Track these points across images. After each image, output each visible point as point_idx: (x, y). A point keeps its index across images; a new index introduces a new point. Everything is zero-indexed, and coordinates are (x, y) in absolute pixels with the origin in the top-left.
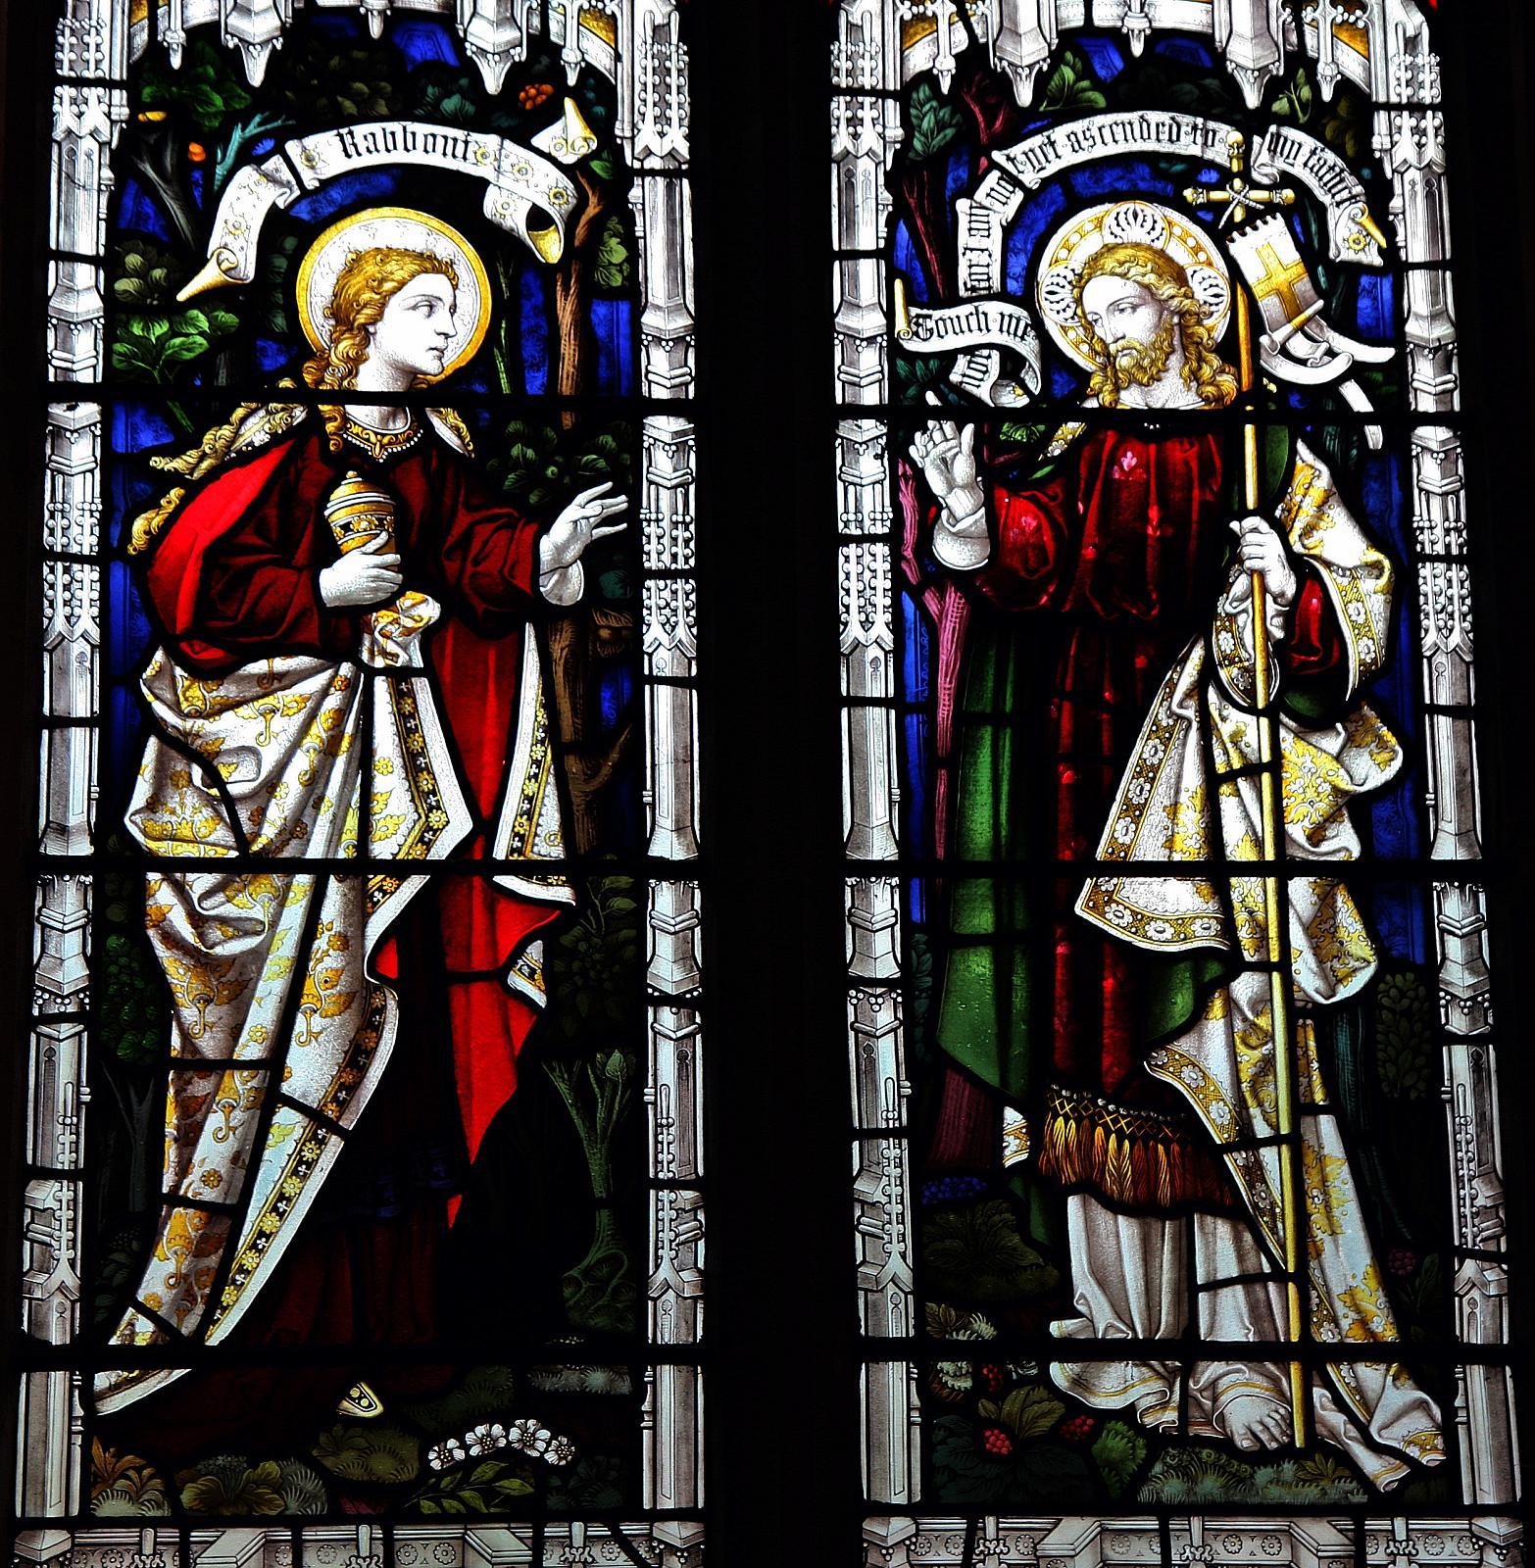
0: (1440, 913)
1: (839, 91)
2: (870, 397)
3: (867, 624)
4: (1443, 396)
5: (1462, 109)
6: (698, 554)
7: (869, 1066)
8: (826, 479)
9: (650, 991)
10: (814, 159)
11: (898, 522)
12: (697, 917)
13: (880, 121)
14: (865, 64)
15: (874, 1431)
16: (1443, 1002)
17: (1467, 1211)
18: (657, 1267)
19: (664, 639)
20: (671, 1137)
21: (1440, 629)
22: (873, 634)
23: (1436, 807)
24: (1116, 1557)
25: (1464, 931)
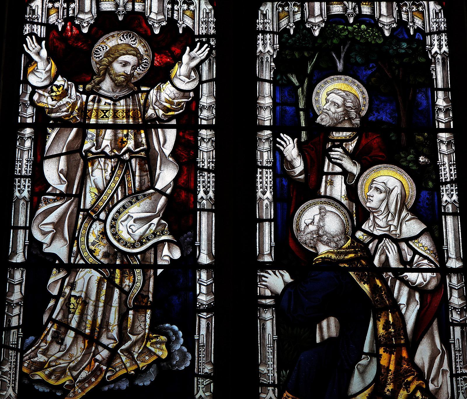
0: (440, 148)
1: (259, 32)
2: (267, 123)
3: (264, 45)
4: (447, 124)
5: (453, 33)
6: (217, 117)
7: (264, 329)
8: (254, 148)
9: (201, 66)
10: (252, 56)
11: (274, 163)
12: (214, 116)
13: (274, 391)
14: (268, 25)
15: (261, 248)
16: (450, 309)
17: (458, 366)
18: (198, 392)
19: (205, 197)
20: (203, 349)
21: (448, 195)
22: (265, 197)
23: (447, 250)
24: (330, 87)
25: (446, 121)
